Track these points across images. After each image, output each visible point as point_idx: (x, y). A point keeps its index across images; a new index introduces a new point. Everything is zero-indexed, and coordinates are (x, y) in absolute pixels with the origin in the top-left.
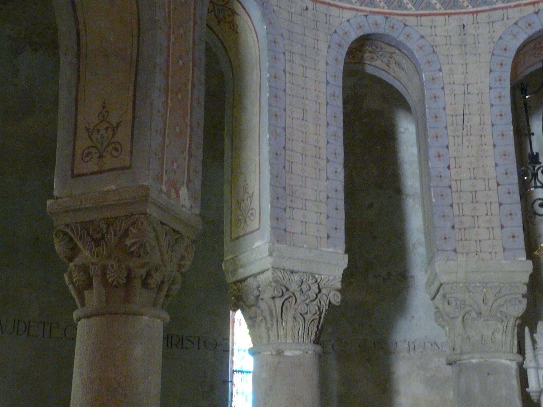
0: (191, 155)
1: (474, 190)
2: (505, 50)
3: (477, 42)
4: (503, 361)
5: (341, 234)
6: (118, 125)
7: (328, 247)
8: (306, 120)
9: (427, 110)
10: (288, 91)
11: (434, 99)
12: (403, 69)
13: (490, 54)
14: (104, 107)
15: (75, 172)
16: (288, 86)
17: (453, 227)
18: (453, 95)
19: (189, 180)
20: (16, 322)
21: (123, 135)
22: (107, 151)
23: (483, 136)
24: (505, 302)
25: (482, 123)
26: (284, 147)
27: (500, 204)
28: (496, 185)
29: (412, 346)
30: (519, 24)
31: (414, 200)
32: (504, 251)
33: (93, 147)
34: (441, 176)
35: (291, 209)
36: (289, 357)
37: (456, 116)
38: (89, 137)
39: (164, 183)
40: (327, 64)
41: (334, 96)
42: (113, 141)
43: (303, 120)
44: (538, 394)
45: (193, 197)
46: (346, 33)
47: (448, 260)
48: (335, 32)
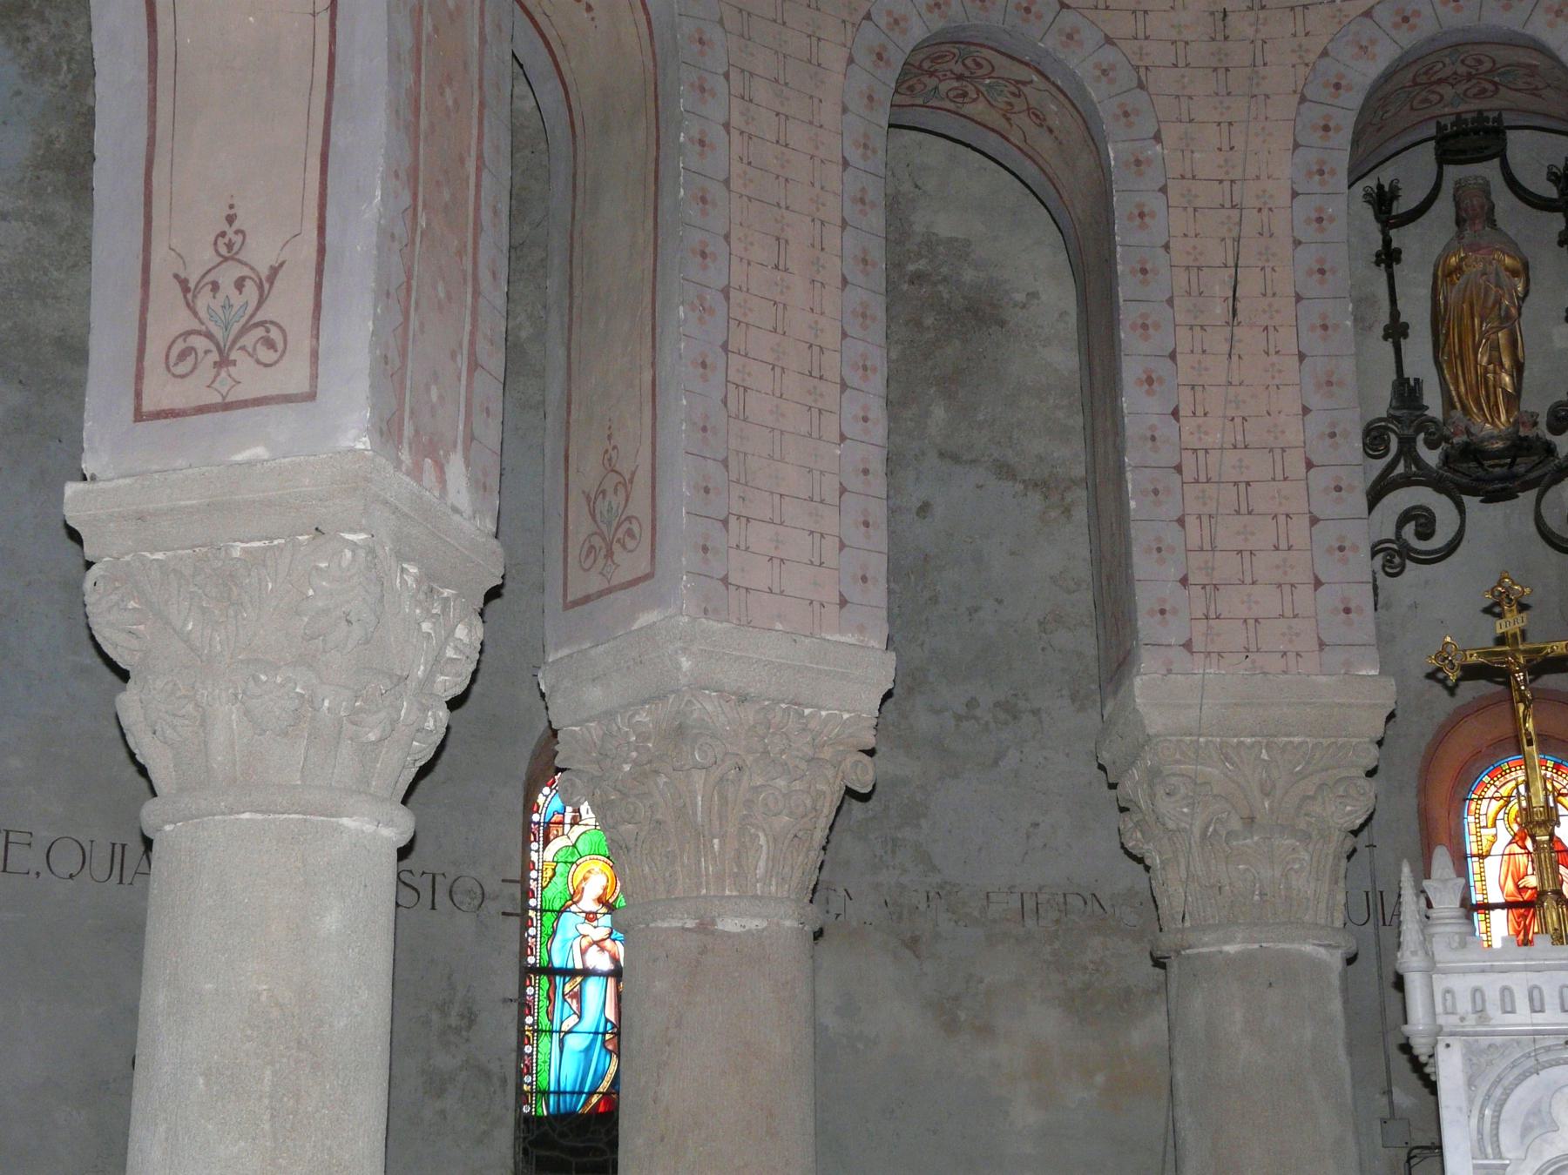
0: (474, 365)
2: (1337, 86)
3: (1259, 62)
4: (1308, 948)
5: (878, 593)
6: (275, 271)
7: (841, 631)
8: (786, 270)
9: (1119, 249)
10: (736, 184)
11: (1138, 221)
12: (1051, 131)
13: (1297, 97)
14: (230, 219)
15: (148, 406)
16: (737, 168)
17: (1184, 581)
18: (1190, 210)
19: (470, 438)
20: (118, 850)
21: (288, 305)
22: (243, 348)
23: (1271, 329)
24: (1321, 787)
25: (1269, 292)
26: (725, 347)
27: (1314, 521)
28: (1303, 465)
29: (1030, 904)
30: (1376, 13)
33: (199, 333)
34: (1153, 438)
35: (743, 520)
36: (729, 935)
37: (1199, 268)
38: (188, 304)
39: (405, 441)
40: (845, 110)
41: (862, 201)
42: (257, 319)
43: (777, 267)
45: (478, 485)
46: (896, 22)
47: (1170, 671)
48: (868, 17)
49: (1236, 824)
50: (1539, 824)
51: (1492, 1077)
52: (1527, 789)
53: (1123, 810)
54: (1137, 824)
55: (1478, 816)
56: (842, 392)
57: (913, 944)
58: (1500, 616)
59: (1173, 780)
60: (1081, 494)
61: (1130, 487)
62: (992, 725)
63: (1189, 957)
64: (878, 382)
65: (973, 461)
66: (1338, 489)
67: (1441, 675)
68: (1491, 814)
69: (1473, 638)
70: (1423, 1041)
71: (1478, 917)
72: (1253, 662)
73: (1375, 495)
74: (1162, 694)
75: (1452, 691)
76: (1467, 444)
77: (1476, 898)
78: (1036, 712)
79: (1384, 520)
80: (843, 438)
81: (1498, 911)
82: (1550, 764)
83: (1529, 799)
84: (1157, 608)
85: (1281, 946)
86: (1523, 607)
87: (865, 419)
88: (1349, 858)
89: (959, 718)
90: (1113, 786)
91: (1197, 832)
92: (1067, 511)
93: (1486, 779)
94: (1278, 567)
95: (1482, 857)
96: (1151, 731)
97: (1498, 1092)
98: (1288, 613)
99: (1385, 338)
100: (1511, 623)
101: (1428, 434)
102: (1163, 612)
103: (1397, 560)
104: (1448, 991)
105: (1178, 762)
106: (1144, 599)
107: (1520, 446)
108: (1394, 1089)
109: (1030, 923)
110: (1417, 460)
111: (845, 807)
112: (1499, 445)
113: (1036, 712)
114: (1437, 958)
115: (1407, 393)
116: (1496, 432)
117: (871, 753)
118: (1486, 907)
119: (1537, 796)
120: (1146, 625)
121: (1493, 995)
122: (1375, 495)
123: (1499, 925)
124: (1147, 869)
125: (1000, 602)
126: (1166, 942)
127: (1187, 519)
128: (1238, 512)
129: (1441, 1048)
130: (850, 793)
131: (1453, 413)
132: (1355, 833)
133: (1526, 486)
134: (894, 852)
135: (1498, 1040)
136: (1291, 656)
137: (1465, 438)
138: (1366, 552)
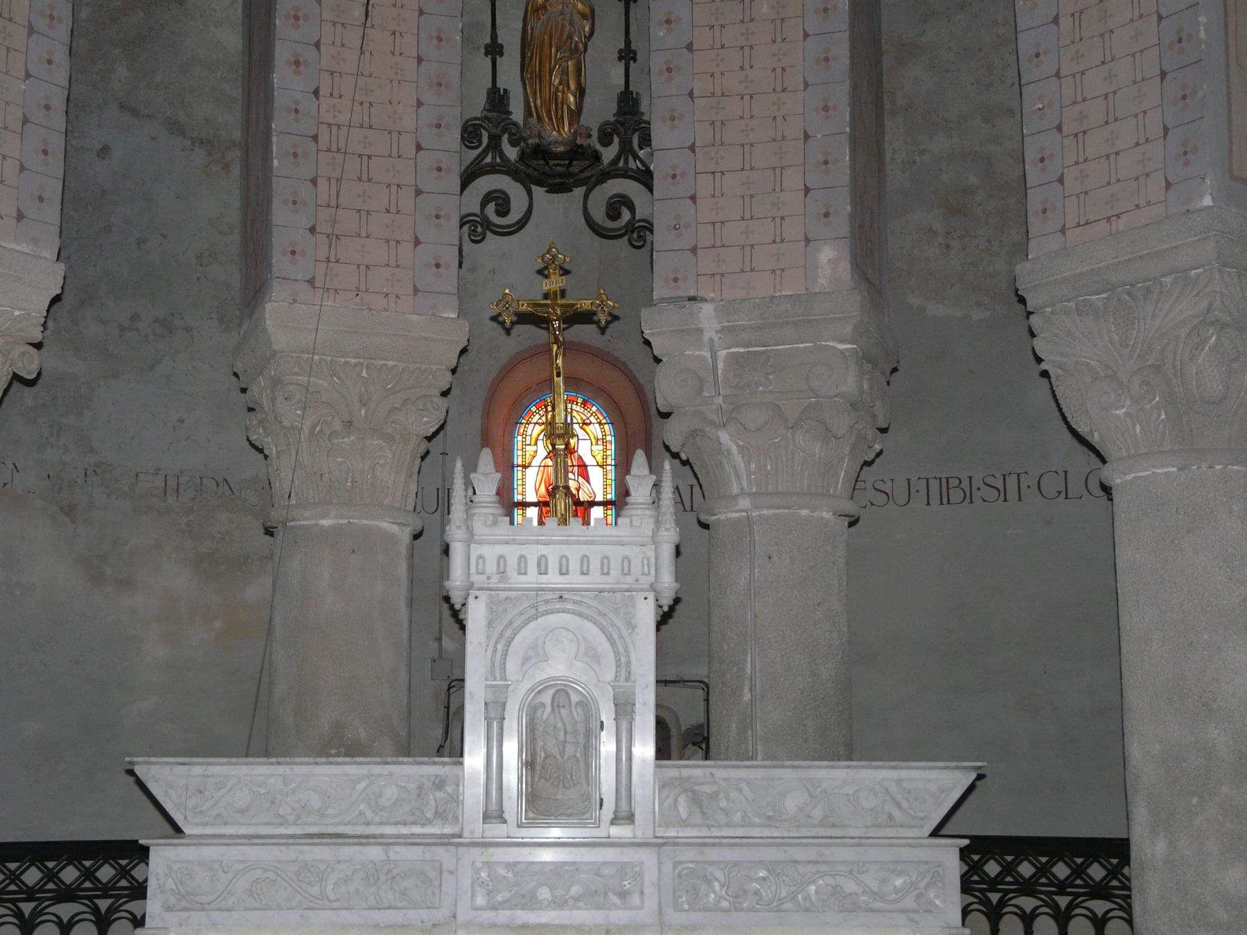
1: (367, 152)
4: (385, 525)
5: (52, 213)
27: (419, 192)
29: (172, 483)
31: (210, 154)
32: (415, 295)
34: (297, 111)
44: (463, 593)
47: (295, 301)
49: (338, 426)
50: (559, 436)
51: (506, 621)
52: (553, 409)
53: (251, 410)
54: (260, 422)
55: (524, 435)
56: (30, 35)
57: (69, 510)
58: (547, 277)
59: (291, 388)
60: (236, 154)
61: (274, 148)
62: (151, 337)
63: (292, 527)
64: (62, 32)
65: (149, 116)
66: (439, 169)
67: (501, 319)
68: (534, 436)
69: (527, 289)
70: (459, 593)
71: (517, 512)
72: (362, 299)
73: (467, 179)
74: (286, 318)
75: (508, 332)
76: (538, 145)
77: (517, 498)
78: (188, 329)
79: (472, 200)
80: (28, 75)
81: (532, 508)
82: (580, 400)
83: (554, 416)
84: (289, 249)
85: (364, 522)
86: (566, 272)
87: (50, 62)
88: (423, 458)
89: (122, 329)
90: (244, 390)
91: (306, 429)
92: (226, 167)
93: (534, 409)
94: (387, 226)
95: (525, 467)
96: (277, 347)
97: (508, 633)
98: (393, 263)
99: (486, 55)
100: (554, 283)
101: (511, 134)
102: (293, 253)
103: (479, 229)
104: (481, 557)
105: (297, 374)
106: (280, 240)
107: (576, 152)
108: (444, 637)
109: (171, 499)
110: (502, 155)
111: (12, 391)
112: (561, 149)
113: (188, 329)
114: (475, 532)
115: (498, 100)
116: (560, 139)
117: (38, 346)
118: (524, 505)
119: (559, 414)
120: (279, 261)
121: (512, 561)
122: (467, 179)
123: (533, 512)
124: (266, 457)
125: (165, 236)
126: (276, 515)
127: (319, 180)
128: (360, 179)
129: (471, 600)
130: (16, 377)
131: (530, 120)
132: (429, 439)
133: (578, 184)
134: (58, 435)
135: (513, 594)
136: (392, 297)
137: (537, 140)
138: (455, 222)
